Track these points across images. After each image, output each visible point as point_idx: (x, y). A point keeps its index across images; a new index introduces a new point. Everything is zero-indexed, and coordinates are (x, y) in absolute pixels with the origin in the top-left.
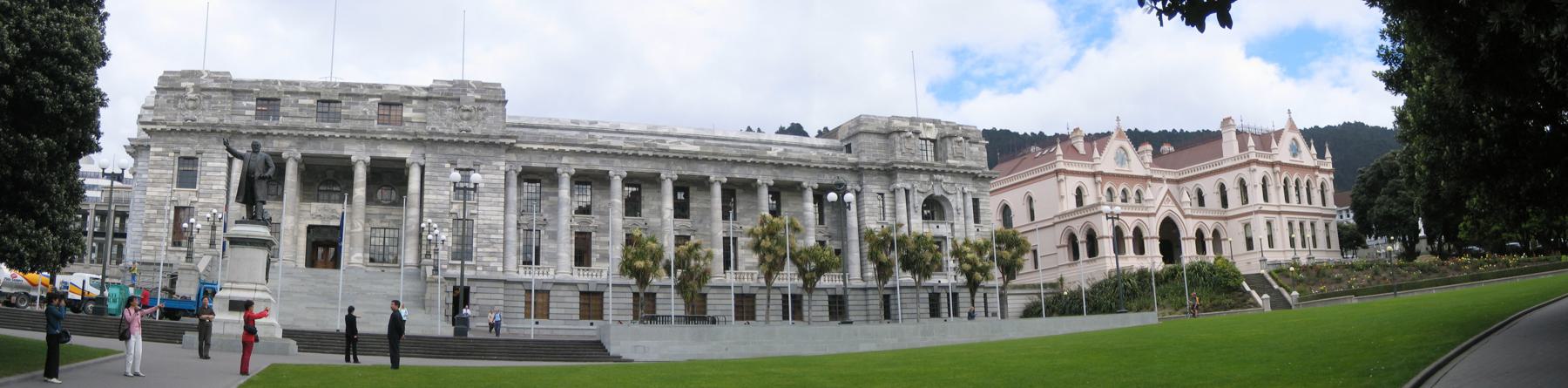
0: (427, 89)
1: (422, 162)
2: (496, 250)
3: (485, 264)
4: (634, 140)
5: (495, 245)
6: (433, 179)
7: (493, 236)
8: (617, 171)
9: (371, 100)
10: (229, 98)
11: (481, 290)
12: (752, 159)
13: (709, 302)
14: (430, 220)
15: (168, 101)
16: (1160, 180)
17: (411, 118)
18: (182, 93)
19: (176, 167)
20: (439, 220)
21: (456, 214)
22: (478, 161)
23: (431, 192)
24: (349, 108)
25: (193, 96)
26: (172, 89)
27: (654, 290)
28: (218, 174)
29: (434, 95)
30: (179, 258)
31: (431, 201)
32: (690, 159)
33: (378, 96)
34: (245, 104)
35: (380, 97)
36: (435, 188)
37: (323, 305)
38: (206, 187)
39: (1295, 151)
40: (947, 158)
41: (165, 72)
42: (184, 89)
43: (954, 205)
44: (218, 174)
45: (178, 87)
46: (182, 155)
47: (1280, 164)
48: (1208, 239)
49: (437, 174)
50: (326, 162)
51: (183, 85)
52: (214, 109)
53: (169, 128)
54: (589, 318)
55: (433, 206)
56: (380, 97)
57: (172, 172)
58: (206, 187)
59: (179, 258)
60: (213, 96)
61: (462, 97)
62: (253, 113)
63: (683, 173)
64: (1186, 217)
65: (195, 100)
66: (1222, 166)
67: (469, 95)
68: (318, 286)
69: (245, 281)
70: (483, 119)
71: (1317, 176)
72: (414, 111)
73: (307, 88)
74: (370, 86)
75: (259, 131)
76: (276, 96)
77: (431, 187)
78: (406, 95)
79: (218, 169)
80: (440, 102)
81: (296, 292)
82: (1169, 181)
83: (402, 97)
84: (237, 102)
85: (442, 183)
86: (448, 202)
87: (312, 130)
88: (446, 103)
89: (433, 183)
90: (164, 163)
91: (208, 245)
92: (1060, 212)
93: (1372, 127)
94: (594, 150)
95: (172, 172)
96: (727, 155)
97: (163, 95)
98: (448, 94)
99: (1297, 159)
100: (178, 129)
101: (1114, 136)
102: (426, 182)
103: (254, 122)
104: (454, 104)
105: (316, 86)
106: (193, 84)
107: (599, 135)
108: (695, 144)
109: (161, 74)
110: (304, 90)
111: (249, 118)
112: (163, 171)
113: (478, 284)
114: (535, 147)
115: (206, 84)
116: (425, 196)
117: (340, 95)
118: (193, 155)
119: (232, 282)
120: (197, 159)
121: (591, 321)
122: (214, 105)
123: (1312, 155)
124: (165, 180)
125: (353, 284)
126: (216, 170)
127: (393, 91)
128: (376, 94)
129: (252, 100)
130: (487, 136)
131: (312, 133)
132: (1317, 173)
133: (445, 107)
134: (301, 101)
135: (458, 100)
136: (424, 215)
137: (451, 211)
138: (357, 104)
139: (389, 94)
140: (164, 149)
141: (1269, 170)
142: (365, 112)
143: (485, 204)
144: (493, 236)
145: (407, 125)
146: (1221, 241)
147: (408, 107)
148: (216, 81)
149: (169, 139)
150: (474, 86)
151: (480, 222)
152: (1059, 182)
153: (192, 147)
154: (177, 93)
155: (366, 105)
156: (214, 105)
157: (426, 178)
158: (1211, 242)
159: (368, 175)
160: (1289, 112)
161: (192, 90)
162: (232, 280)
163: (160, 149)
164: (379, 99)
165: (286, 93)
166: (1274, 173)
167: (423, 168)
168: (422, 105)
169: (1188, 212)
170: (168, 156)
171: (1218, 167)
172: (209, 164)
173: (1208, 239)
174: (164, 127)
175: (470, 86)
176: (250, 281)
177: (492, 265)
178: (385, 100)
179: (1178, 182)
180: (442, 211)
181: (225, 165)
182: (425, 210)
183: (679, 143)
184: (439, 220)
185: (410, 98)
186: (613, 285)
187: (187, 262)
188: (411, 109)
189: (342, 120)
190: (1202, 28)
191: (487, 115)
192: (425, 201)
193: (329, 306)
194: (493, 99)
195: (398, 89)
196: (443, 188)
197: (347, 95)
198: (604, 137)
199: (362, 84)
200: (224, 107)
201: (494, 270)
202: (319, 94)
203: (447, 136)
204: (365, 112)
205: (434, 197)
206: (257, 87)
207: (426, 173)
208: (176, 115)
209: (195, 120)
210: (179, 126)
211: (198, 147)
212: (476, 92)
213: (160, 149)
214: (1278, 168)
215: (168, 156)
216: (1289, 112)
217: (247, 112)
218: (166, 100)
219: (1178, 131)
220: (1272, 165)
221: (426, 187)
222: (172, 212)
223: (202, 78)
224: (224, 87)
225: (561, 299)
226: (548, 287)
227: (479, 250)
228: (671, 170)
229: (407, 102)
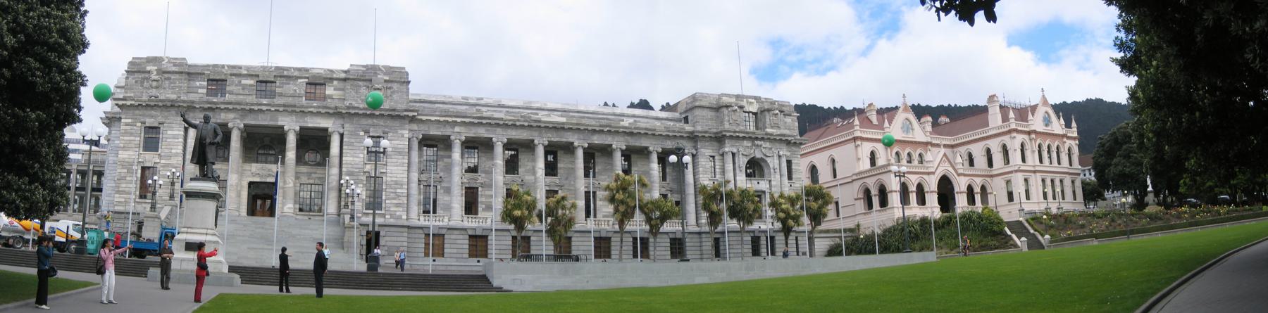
0: (346, 72)
1: (341, 131)
2: (401, 202)
3: (392, 213)
4: (513, 113)
5: (400, 198)
6: (350, 144)
7: (398, 191)
8: (499, 138)
9: (300, 81)
10: (185, 79)
11: (389, 234)
12: (608, 129)
13: (573, 243)
14: (348, 178)
15: (136, 82)
16: (938, 145)
17: (332, 95)
18: (147, 75)
19: (143, 135)
20: (355, 178)
21: (369, 172)
22: (386, 130)
23: (349, 155)
24: (282, 87)
25: (156, 77)
26: (139, 72)
27: (529, 234)
28: (177, 141)
29: (351, 77)
30: (145, 208)
31: (348, 162)
32: (558, 128)
33: (305, 78)
34: (198, 84)
35: (308, 78)
36: (352, 152)
37: (261, 246)
38: (166, 151)
39: (1047, 121)
40: (766, 128)
41: (133, 58)
42: (149, 72)
43: (771, 166)
44: (177, 141)
45: (144, 70)
46: (147, 125)
47: (1035, 132)
48: (977, 193)
49: (353, 141)
50: (264, 131)
51: (148, 68)
52: (173, 88)
53: (137, 103)
54: (476, 257)
55: (350, 166)
56: (308, 78)
57: (139, 139)
58: (166, 151)
59: (145, 208)
60: (173, 77)
61: (373, 78)
62: (205, 91)
63: (553, 139)
64: (959, 175)
65: (157, 81)
66: (988, 134)
67: (379, 76)
68: (257, 230)
69: (198, 226)
70: (391, 96)
71: (1065, 142)
72: (335, 90)
73: (248, 71)
74: (299, 70)
75: (209, 106)
76: (223, 77)
77: (348, 151)
78: (329, 76)
79: (176, 137)
80: (356, 82)
81: (240, 236)
82: (945, 146)
83: (325, 78)
84: (192, 82)
85: (357, 148)
86: (362, 163)
87: (252, 105)
88: (361, 83)
89: (350, 147)
90: (133, 131)
91: (168, 198)
92: (857, 171)
93: (1110, 103)
94: (480, 121)
95: (139, 139)
96: (588, 125)
97: (132, 77)
98: (362, 76)
99: (1049, 128)
100: (144, 104)
101: (901, 110)
102: (344, 147)
103: (205, 98)
104: (367, 84)
105: (256, 70)
106: (156, 68)
107: (484, 109)
108: (562, 116)
109: (130, 60)
110: (246, 72)
111: (201, 95)
112: (132, 138)
113: (387, 229)
114: (433, 119)
115: (166, 68)
116: (344, 158)
117: (275, 76)
118: (156, 125)
119: (188, 228)
120: (160, 128)
121: (478, 259)
122: (173, 85)
123: (1061, 125)
124: (133, 146)
125: (285, 229)
126: (175, 137)
127: (318, 73)
128: (304, 75)
129: (204, 81)
130: (394, 110)
131: (253, 107)
132: (1065, 140)
133: (360, 86)
134: (244, 82)
135: (371, 80)
136: (343, 173)
137: (365, 170)
138: (289, 84)
139: (314, 76)
140: (133, 121)
141: (1026, 137)
142: (295, 90)
143: (393, 164)
144: (398, 191)
145: (329, 100)
146: (987, 194)
147: (330, 86)
148: (174, 65)
149: (137, 112)
150: (383, 69)
151: (389, 179)
152: (857, 147)
153: (155, 119)
154: (143, 75)
155: (296, 85)
156: (173, 85)
157: (344, 143)
158: (979, 195)
159: (298, 141)
160: (1043, 90)
161: (155, 73)
162: (188, 226)
163: (130, 121)
164: (307, 80)
165: (231, 75)
166: (1030, 140)
167: (342, 136)
168: (341, 85)
169: (961, 171)
170: (136, 126)
171: (985, 135)
172: (169, 132)
173: (977, 193)
174: (133, 102)
175: (380, 69)
176: (202, 227)
177: (398, 213)
178: (311, 81)
179: (952, 147)
180: (357, 170)
181: (182, 133)
182: (344, 169)
183: (549, 115)
184: (355, 178)
185: (332, 79)
186: (496, 230)
187: (151, 211)
188: (333, 88)
189: (277, 97)
190: (972, 23)
191: (393, 92)
192: (344, 162)
193: (266, 247)
194: (398, 80)
195: (322, 71)
196: (358, 152)
197: (281, 77)
198: (488, 110)
199: (293, 68)
200: (181, 87)
201: (400, 217)
202: (258, 76)
203: (361, 110)
204: (295, 90)
205: (351, 159)
206: (208, 70)
207: (345, 140)
208: (143, 92)
209: (158, 97)
210: (145, 102)
211: (160, 119)
212: (385, 74)
213: (130, 121)
214: (1033, 136)
215: (136, 126)
216: (1043, 90)
217: (200, 91)
218: (134, 81)
219: (953, 106)
220: (1029, 133)
221: (344, 151)
222: (139, 171)
223: (163, 63)
224: (181, 70)
225: (454, 242)
226: (443, 232)
227: (387, 202)
228: (542, 137)
229: (329, 82)
